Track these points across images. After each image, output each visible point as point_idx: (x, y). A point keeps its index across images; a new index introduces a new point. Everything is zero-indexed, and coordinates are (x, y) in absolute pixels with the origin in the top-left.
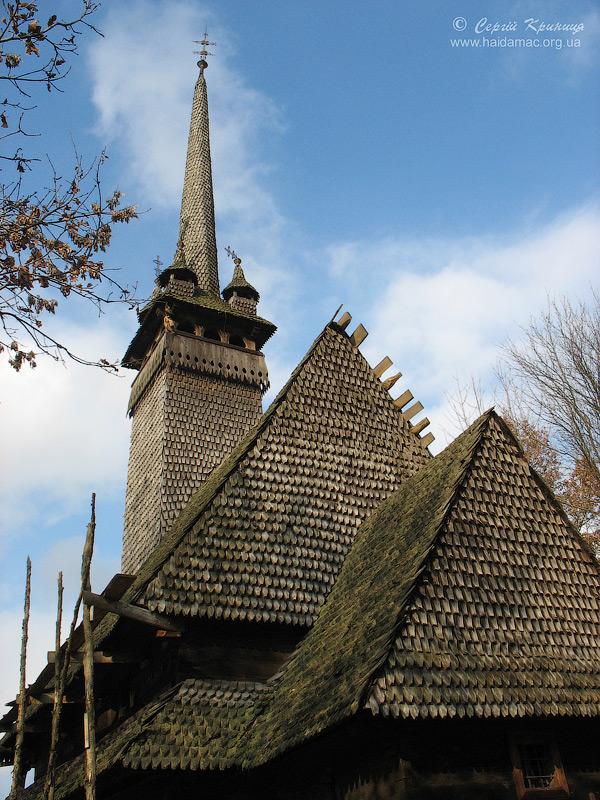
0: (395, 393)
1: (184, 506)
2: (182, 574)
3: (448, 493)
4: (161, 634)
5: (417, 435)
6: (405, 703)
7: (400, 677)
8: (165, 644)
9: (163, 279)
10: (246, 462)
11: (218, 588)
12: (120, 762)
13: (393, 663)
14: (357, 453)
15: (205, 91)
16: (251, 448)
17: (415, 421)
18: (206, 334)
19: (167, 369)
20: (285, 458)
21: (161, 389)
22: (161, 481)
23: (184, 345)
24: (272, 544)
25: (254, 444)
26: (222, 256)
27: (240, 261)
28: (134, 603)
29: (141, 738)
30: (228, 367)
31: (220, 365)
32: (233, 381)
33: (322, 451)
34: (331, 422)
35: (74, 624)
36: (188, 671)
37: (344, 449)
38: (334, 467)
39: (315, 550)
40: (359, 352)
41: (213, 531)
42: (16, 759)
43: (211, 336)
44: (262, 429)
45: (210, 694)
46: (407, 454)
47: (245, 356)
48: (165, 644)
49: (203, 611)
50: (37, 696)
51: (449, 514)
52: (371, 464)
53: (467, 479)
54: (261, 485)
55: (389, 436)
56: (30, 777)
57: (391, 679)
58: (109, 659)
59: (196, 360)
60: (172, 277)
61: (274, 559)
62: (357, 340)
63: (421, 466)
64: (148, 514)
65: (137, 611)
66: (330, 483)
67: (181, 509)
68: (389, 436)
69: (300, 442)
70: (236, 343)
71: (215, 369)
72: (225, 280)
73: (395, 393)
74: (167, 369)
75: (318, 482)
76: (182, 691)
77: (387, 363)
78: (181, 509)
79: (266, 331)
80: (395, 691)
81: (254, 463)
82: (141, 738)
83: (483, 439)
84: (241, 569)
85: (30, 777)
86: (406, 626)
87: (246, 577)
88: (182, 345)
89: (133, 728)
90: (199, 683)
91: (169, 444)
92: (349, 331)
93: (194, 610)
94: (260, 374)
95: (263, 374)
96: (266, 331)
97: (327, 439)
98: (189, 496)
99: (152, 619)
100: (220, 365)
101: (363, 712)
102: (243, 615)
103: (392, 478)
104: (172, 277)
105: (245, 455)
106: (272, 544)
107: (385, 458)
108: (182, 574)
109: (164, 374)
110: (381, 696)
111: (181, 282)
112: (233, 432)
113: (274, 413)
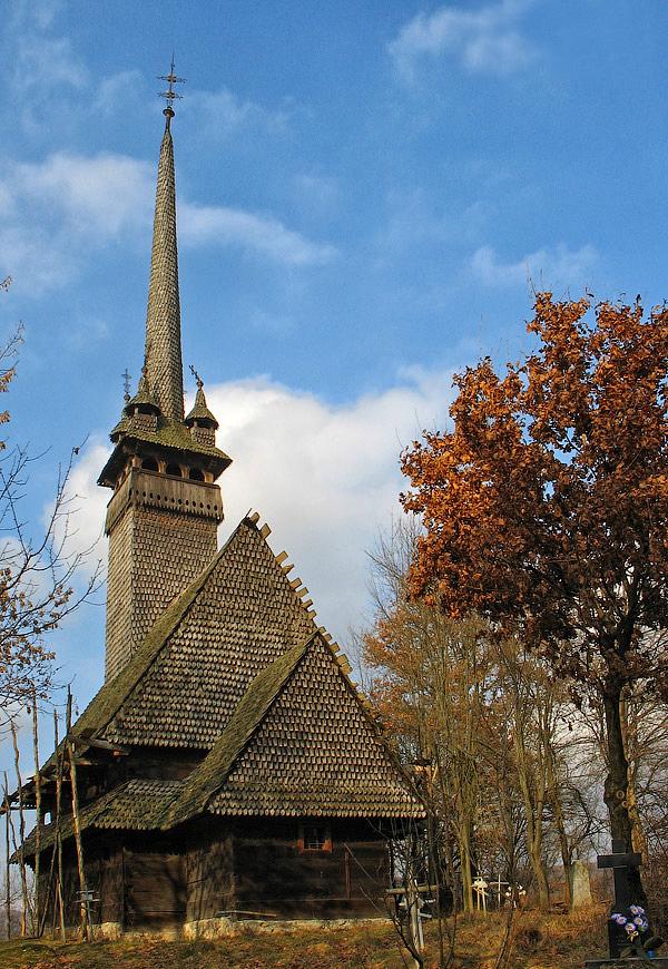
0: (291, 577)
1: (149, 629)
2: (128, 719)
3: (276, 690)
4: (115, 753)
5: (306, 609)
6: (234, 809)
7: (228, 795)
8: (118, 760)
9: (129, 411)
10: (172, 640)
11: (151, 727)
12: (93, 825)
13: (225, 788)
14: (254, 628)
15: (171, 154)
16: (176, 630)
17: (304, 599)
18: (169, 470)
19: (134, 507)
20: (200, 637)
21: (128, 525)
22: (131, 609)
23: (148, 483)
24: (188, 698)
25: (178, 626)
26: (186, 371)
27: (202, 384)
28: (98, 738)
29: (106, 812)
30: (187, 503)
31: (180, 502)
32: (191, 515)
33: (227, 629)
34: (237, 605)
35: (56, 741)
36: (133, 774)
37: (245, 627)
38: (236, 640)
39: (186, 734)
40: (266, 543)
41: (149, 689)
42: (38, 802)
43: (173, 471)
44: (185, 615)
45: (146, 788)
46: (295, 625)
47: (203, 490)
48: (118, 760)
49: (141, 742)
50: (47, 777)
51: (273, 705)
52: (264, 637)
53: (290, 680)
54: (182, 656)
55: (282, 612)
56: (48, 816)
57: (223, 795)
58: (86, 763)
59: (159, 497)
60: (136, 410)
61: (188, 707)
62: (264, 534)
63: (304, 635)
64: (120, 633)
65: (100, 742)
66: (231, 653)
67: (147, 632)
68: (282, 612)
69: (213, 623)
70: (196, 477)
71: (175, 505)
72: (189, 406)
73: (291, 577)
74: (134, 507)
75: (223, 652)
76: (130, 786)
77: (284, 555)
78: (147, 632)
79: (222, 463)
80: (225, 802)
81: (177, 642)
82: (106, 812)
83: (307, 654)
84: (166, 714)
85: (48, 818)
86: (237, 769)
87: (169, 720)
88: (146, 484)
89: (100, 808)
90: (140, 782)
91: (136, 577)
92: (259, 525)
93: (136, 740)
94: (216, 508)
95: (219, 507)
96: (222, 463)
97: (232, 619)
98: (154, 621)
99: (110, 747)
100: (180, 502)
101: (206, 812)
102: (166, 743)
103: (280, 646)
104: (136, 410)
105: (171, 635)
106: (188, 698)
107: (275, 631)
108: (128, 719)
109: (131, 511)
110: (216, 804)
111: (144, 416)
112: (191, 563)
113: (194, 601)
